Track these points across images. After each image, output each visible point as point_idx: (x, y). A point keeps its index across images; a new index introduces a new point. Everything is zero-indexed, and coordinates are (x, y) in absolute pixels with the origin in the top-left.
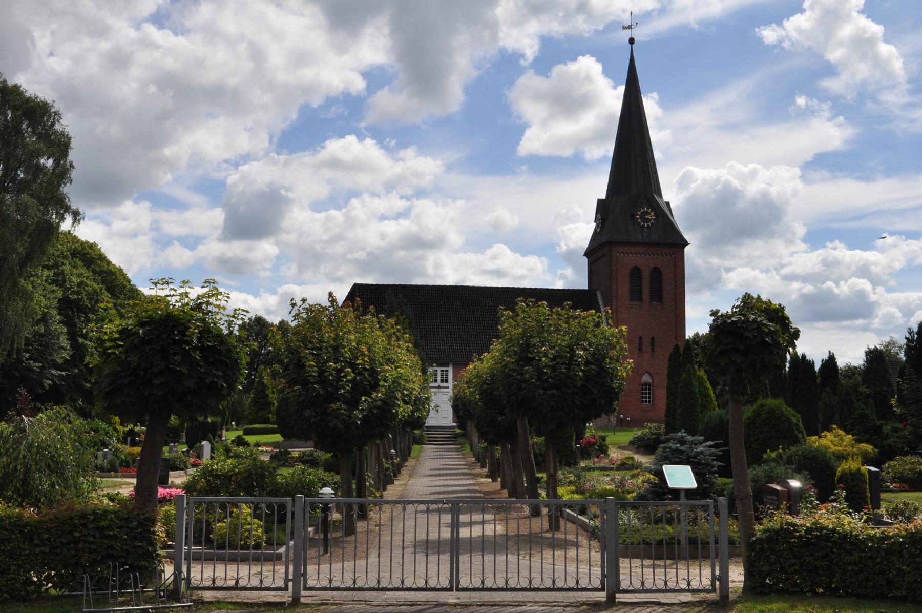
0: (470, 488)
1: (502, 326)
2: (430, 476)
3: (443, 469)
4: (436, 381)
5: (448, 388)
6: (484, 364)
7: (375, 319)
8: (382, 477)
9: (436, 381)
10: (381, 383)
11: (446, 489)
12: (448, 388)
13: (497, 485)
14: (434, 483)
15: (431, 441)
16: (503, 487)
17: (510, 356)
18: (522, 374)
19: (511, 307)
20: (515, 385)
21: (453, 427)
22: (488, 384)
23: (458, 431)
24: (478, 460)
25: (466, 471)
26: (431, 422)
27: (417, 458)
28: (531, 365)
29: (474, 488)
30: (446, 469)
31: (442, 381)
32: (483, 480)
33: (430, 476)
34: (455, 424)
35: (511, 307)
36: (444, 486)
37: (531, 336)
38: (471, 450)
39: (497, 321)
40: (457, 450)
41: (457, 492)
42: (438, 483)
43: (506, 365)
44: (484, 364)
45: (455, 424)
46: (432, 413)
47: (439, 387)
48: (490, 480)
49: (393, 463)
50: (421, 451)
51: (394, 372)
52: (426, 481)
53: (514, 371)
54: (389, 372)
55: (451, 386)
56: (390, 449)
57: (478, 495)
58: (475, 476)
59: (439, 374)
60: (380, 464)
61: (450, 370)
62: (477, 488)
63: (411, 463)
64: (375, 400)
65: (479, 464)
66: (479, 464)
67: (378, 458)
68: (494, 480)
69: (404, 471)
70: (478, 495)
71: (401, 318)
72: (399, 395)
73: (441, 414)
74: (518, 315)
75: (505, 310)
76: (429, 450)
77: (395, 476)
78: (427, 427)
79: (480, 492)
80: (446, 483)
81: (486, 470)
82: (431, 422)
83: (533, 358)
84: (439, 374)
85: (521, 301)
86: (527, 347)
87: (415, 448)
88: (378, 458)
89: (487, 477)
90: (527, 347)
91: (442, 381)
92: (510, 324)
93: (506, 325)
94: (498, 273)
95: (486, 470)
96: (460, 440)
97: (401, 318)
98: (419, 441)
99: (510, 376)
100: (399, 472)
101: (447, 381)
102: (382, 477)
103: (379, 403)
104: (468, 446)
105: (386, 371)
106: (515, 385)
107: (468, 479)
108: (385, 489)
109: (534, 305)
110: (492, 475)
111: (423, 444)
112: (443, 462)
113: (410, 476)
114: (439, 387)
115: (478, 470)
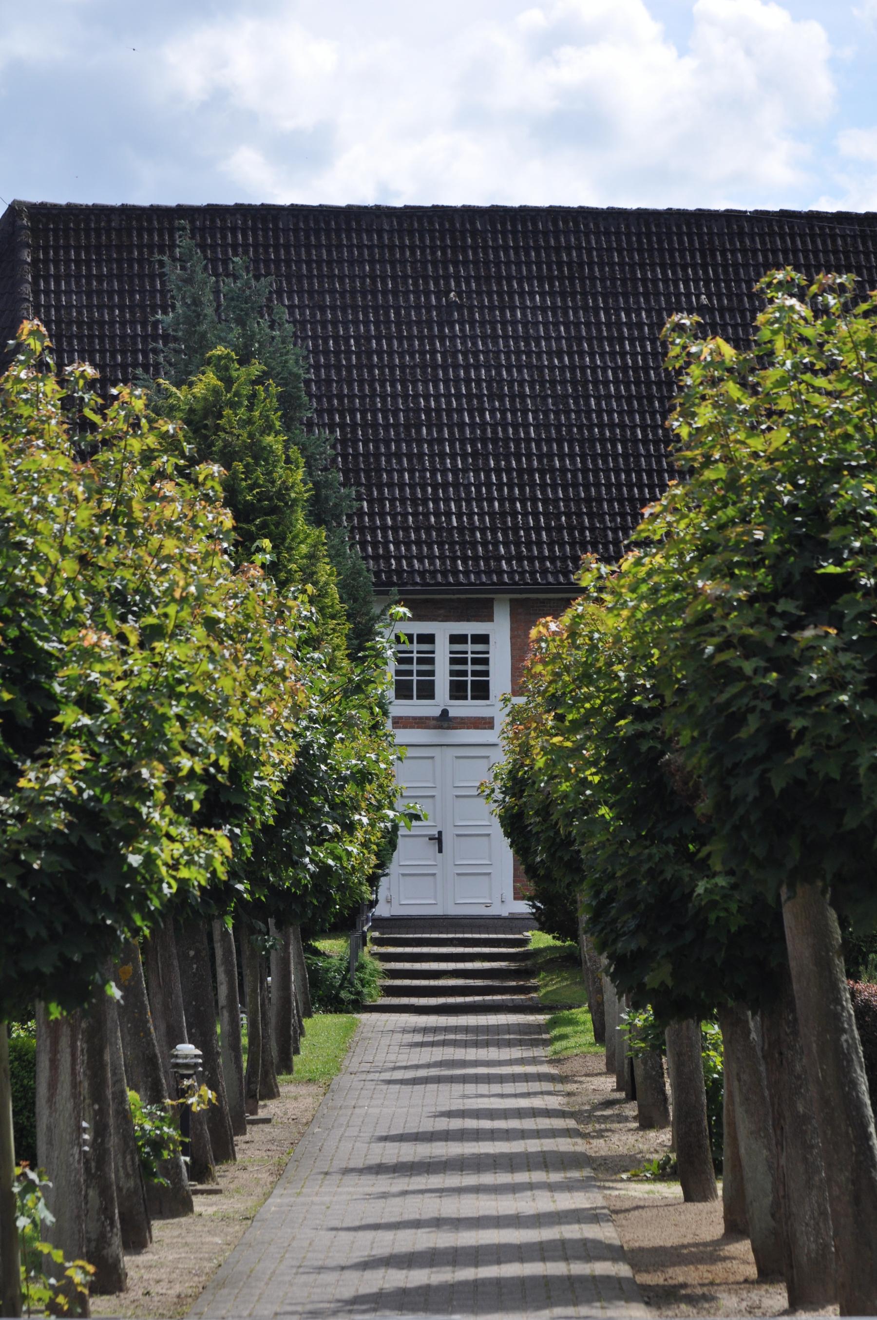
0: (572, 1232)
1: (689, 415)
2: (379, 1169)
3: (446, 1136)
4: (427, 691)
5: (487, 723)
6: (611, 607)
7: (50, 386)
8: (117, 1171)
9: (427, 691)
10: (70, 717)
11: (444, 1239)
12: (487, 723)
13: (708, 1219)
14: (395, 1210)
15: (402, 995)
16: (735, 1228)
17: (726, 572)
18: (788, 666)
19: (734, 318)
20: (753, 723)
21: (513, 922)
22: (640, 714)
23: (540, 940)
24: (629, 1087)
25: (564, 1145)
26: (399, 895)
27: (323, 1081)
28: (837, 620)
29: (591, 1232)
30: (462, 1135)
31: (458, 691)
32: (639, 1191)
33: (379, 1169)
34: (523, 908)
35: (734, 318)
36: (438, 1223)
37: (836, 470)
38: (600, 1036)
39: (661, 389)
40: (530, 1037)
41: (520, 1253)
42: (413, 1208)
43: (705, 618)
44: (611, 607)
45: (523, 908)
46: (409, 853)
47: (444, 721)
48: (674, 1190)
49: (184, 1118)
50: (347, 1043)
51: (137, 661)
52: (354, 1200)
53: (749, 647)
54: (100, 661)
55: (501, 718)
56: (174, 1038)
57: (602, 1268)
58: (610, 1167)
59: (442, 651)
60: (109, 1117)
61: (499, 630)
62: (605, 1233)
63: (291, 1100)
64: (35, 805)
65: (631, 1110)
66: (631, 1110)
67: (99, 1093)
68: (695, 1192)
69: (252, 1145)
70: (602, 1268)
71: (240, 373)
72: (153, 775)
73: (452, 857)
74: (767, 359)
75: (701, 332)
76: (385, 1036)
77: (200, 1172)
78: (380, 923)
79: (615, 1253)
80: (451, 1207)
81: (665, 1136)
82: (399, 895)
83: (845, 583)
84: (442, 651)
85: (787, 287)
86: (812, 524)
87: (320, 1028)
88: (99, 1093)
89: (664, 1173)
90: (812, 524)
91: (458, 691)
92: (734, 403)
93: (706, 414)
94: (579, 123)
95: (665, 1136)
96: (547, 985)
97: (240, 373)
98: (337, 996)
99: (732, 674)
100: (225, 1153)
101: (482, 691)
102: (117, 1171)
103: (58, 819)
104: (583, 1015)
105: (88, 655)
106: (753, 723)
107: (568, 1187)
108: (137, 1242)
109: (846, 309)
110: (689, 1169)
111: (359, 1006)
112: (451, 1097)
113: (280, 1172)
114: (444, 721)
115: (625, 1140)
